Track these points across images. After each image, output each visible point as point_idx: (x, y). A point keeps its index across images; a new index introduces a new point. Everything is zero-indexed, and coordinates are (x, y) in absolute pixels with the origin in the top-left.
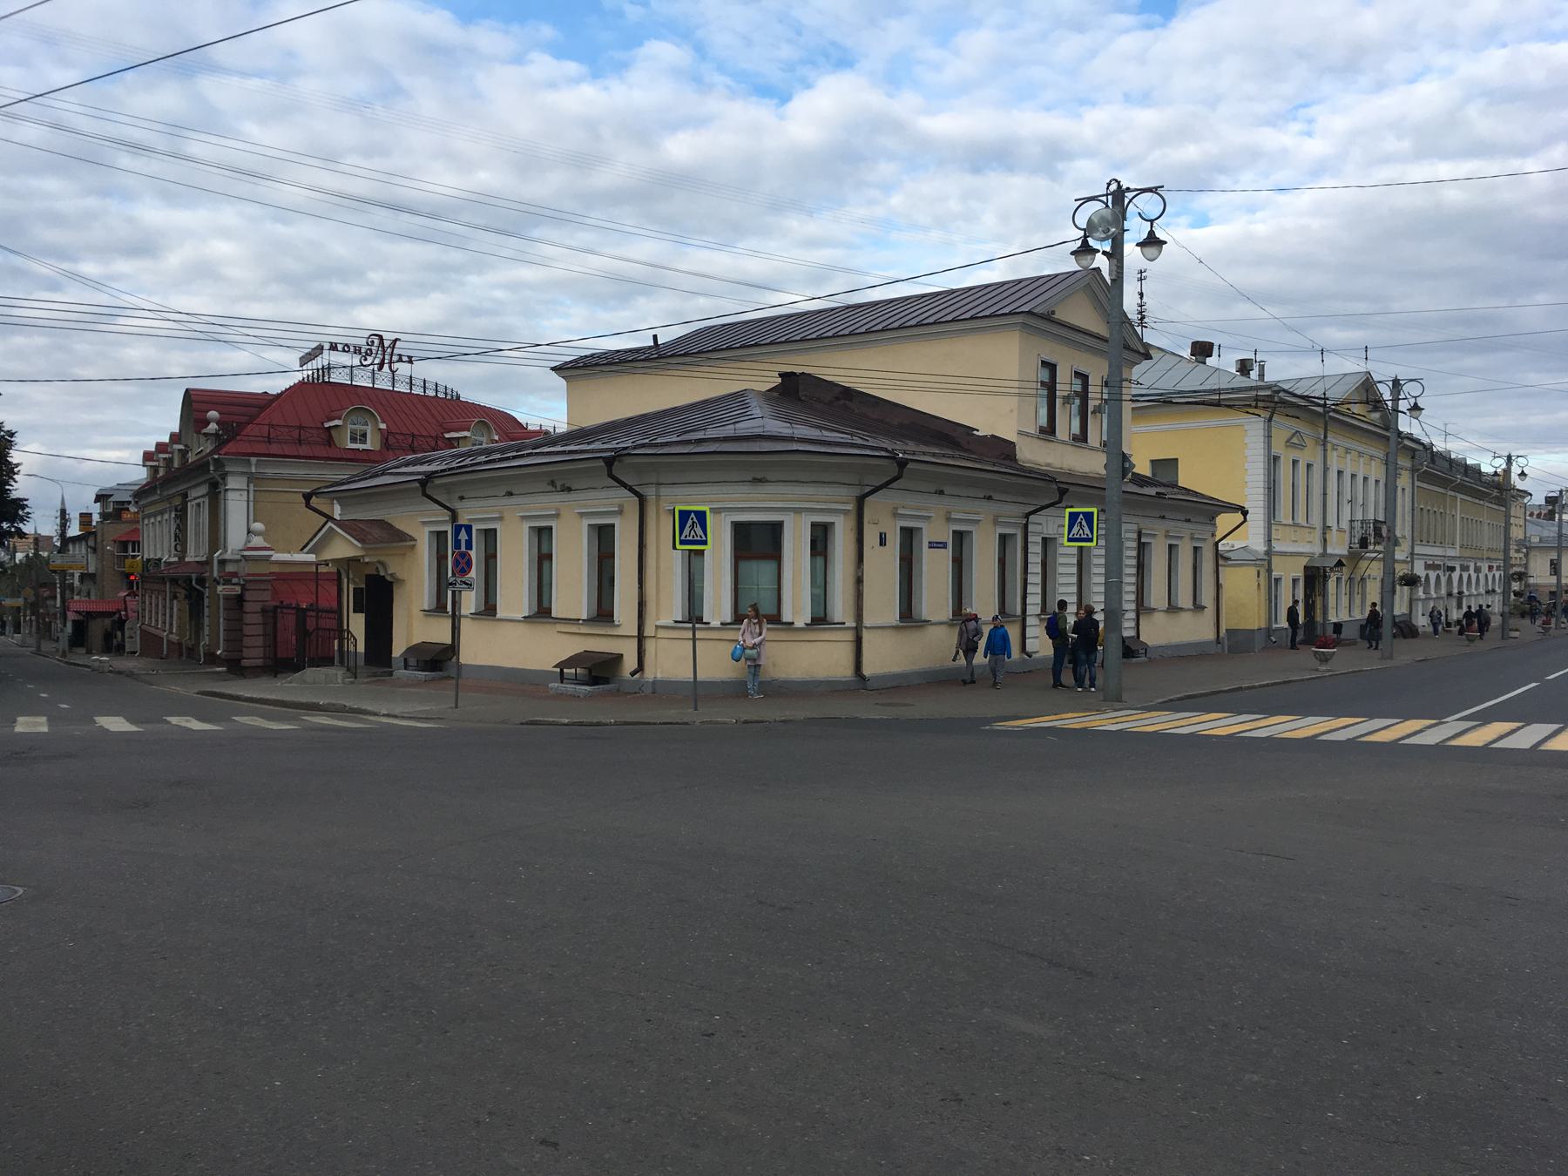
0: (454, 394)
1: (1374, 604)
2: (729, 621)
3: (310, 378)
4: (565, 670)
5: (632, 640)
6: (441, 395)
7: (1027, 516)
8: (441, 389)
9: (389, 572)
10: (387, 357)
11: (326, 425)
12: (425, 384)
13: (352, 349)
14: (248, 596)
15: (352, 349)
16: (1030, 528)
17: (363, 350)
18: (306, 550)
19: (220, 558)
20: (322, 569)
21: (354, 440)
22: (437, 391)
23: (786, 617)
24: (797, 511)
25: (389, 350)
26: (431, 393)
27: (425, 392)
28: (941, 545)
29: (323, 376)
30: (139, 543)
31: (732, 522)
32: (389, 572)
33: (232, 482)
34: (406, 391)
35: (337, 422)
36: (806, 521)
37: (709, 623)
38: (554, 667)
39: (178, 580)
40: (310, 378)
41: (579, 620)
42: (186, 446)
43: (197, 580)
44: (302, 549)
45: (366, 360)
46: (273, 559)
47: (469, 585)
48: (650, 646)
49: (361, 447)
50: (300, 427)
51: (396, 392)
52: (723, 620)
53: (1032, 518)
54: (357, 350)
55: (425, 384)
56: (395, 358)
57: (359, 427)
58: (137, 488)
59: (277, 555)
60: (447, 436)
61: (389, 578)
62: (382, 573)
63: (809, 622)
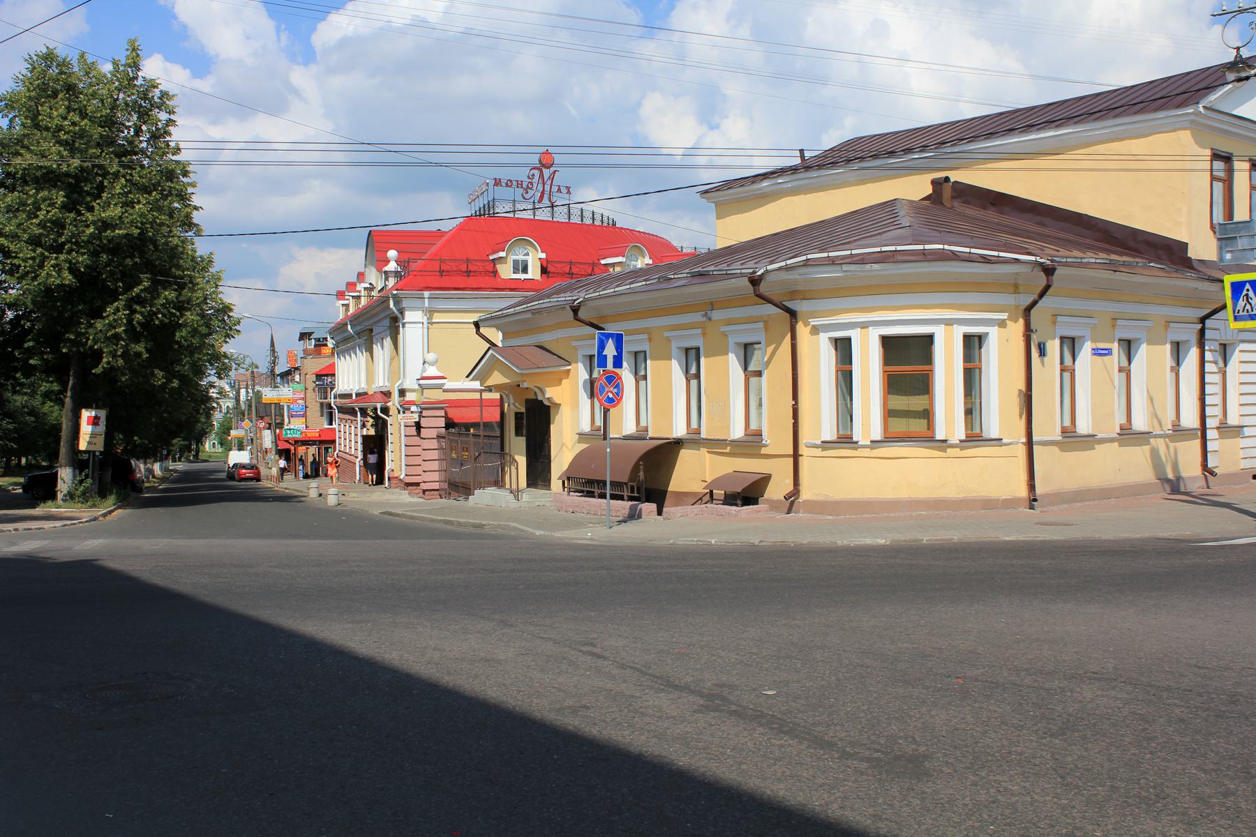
0: (611, 222)
1: (302, 456)
2: (879, 438)
3: (482, 210)
4: (714, 491)
5: (1211, 438)
6: (598, 223)
7: (1203, 320)
8: (598, 217)
9: (546, 397)
10: (547, 188)
11: (491, 258)
12: (593, 215)
13: (515, 183)
14: (424, 423)
15: (515, 183)
16: (1208, 334)
17: (524, 186)
18: (471, 377)
19: (400, 388)
20: (486, 396)
21: (516, 271)
22: (593, 221)
23: (940, 435)
24: (949, 322)
25: (549, 182)
26: (588, 221)
27: (582, 220)
28: (1107, 352)
29: (489, 211)
30: (980, 369)
31: (880, 335)
32: (546, 397)
33: (409, 316)
34: (578, 222)
35: (502, 254)
36: (959, 331)
37: (857, 443)
38: (704, 489)
39: (367, 409)
40: (482, 210)
41: (727, 440)
42: (370, 284)
43: (381, 408)
44: (467, 377)
45: (527, 193)
46: (445, 387)
47: (201, 414)
48: (804, 463)
49: (522, 276)
50: (468, 260)
51: (571, 223)
52: (823, 439)
53: (1208, 322)
54: (520, 184)
55: (593, 215)
56: (555, 189)
57: (520, 257)
58: (332, 325)
59: (450, 383)
60: (603, 262)
61: (546, 403)
62: (540, 399)
63: (963, 437)
